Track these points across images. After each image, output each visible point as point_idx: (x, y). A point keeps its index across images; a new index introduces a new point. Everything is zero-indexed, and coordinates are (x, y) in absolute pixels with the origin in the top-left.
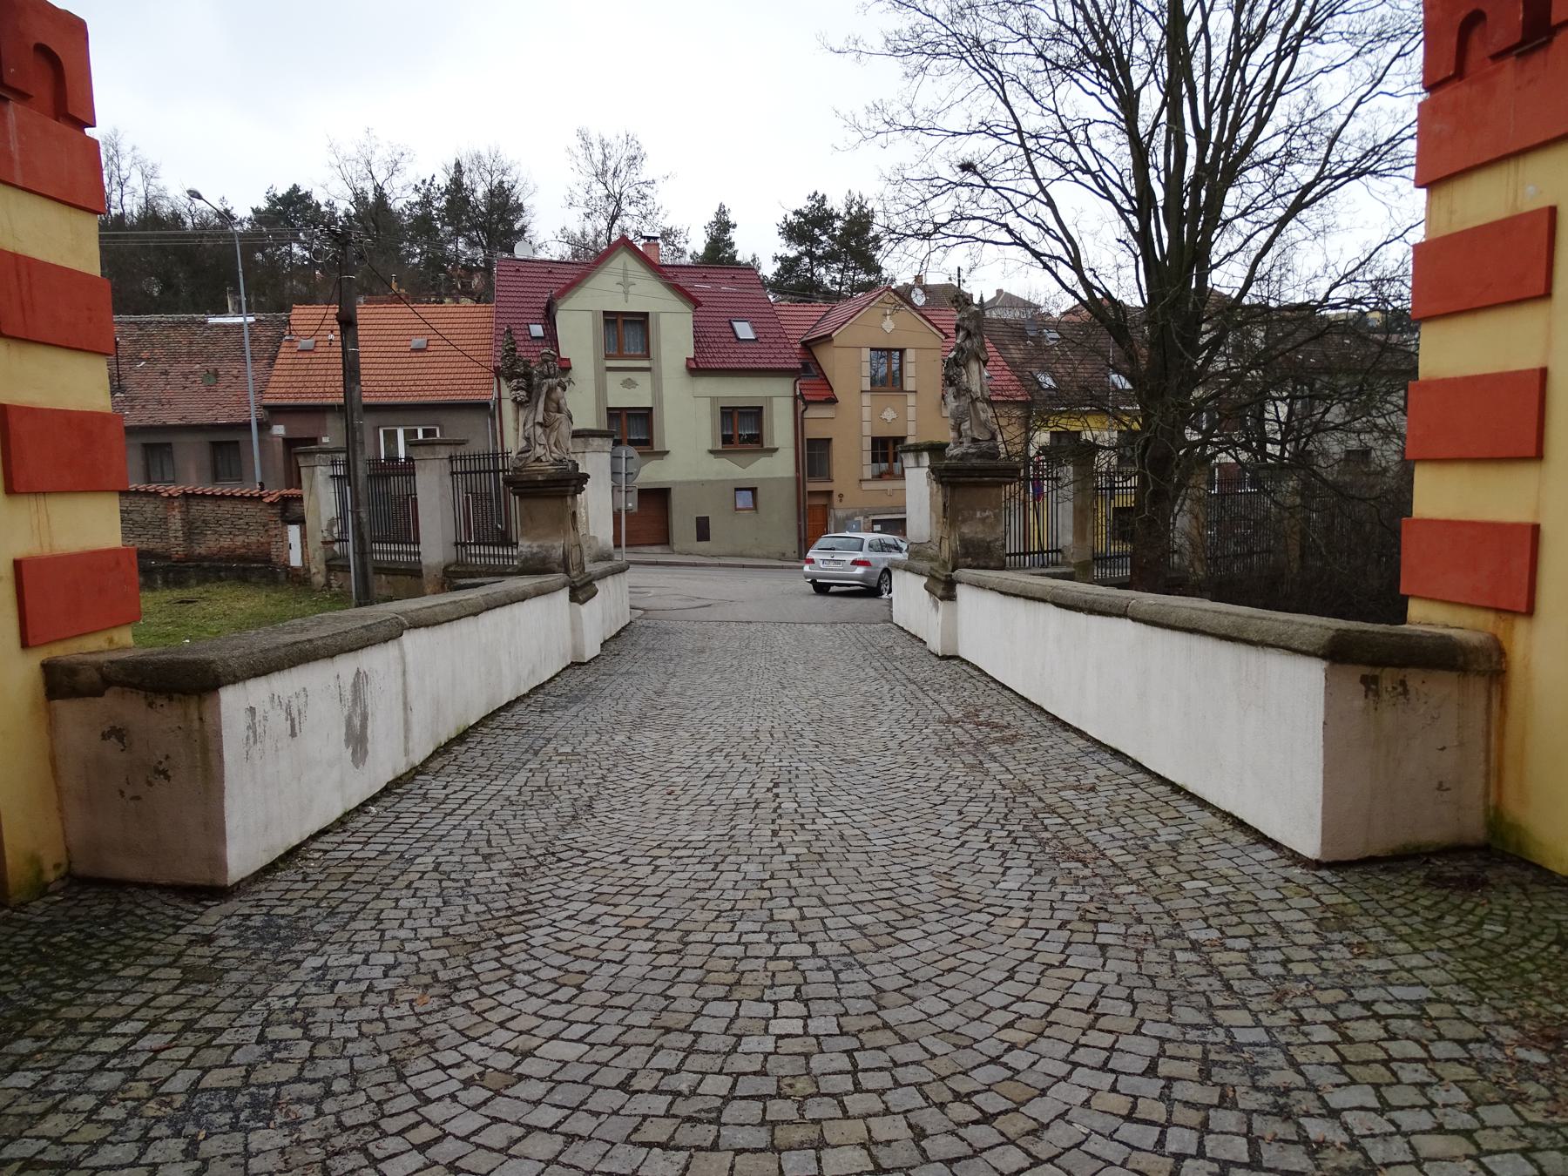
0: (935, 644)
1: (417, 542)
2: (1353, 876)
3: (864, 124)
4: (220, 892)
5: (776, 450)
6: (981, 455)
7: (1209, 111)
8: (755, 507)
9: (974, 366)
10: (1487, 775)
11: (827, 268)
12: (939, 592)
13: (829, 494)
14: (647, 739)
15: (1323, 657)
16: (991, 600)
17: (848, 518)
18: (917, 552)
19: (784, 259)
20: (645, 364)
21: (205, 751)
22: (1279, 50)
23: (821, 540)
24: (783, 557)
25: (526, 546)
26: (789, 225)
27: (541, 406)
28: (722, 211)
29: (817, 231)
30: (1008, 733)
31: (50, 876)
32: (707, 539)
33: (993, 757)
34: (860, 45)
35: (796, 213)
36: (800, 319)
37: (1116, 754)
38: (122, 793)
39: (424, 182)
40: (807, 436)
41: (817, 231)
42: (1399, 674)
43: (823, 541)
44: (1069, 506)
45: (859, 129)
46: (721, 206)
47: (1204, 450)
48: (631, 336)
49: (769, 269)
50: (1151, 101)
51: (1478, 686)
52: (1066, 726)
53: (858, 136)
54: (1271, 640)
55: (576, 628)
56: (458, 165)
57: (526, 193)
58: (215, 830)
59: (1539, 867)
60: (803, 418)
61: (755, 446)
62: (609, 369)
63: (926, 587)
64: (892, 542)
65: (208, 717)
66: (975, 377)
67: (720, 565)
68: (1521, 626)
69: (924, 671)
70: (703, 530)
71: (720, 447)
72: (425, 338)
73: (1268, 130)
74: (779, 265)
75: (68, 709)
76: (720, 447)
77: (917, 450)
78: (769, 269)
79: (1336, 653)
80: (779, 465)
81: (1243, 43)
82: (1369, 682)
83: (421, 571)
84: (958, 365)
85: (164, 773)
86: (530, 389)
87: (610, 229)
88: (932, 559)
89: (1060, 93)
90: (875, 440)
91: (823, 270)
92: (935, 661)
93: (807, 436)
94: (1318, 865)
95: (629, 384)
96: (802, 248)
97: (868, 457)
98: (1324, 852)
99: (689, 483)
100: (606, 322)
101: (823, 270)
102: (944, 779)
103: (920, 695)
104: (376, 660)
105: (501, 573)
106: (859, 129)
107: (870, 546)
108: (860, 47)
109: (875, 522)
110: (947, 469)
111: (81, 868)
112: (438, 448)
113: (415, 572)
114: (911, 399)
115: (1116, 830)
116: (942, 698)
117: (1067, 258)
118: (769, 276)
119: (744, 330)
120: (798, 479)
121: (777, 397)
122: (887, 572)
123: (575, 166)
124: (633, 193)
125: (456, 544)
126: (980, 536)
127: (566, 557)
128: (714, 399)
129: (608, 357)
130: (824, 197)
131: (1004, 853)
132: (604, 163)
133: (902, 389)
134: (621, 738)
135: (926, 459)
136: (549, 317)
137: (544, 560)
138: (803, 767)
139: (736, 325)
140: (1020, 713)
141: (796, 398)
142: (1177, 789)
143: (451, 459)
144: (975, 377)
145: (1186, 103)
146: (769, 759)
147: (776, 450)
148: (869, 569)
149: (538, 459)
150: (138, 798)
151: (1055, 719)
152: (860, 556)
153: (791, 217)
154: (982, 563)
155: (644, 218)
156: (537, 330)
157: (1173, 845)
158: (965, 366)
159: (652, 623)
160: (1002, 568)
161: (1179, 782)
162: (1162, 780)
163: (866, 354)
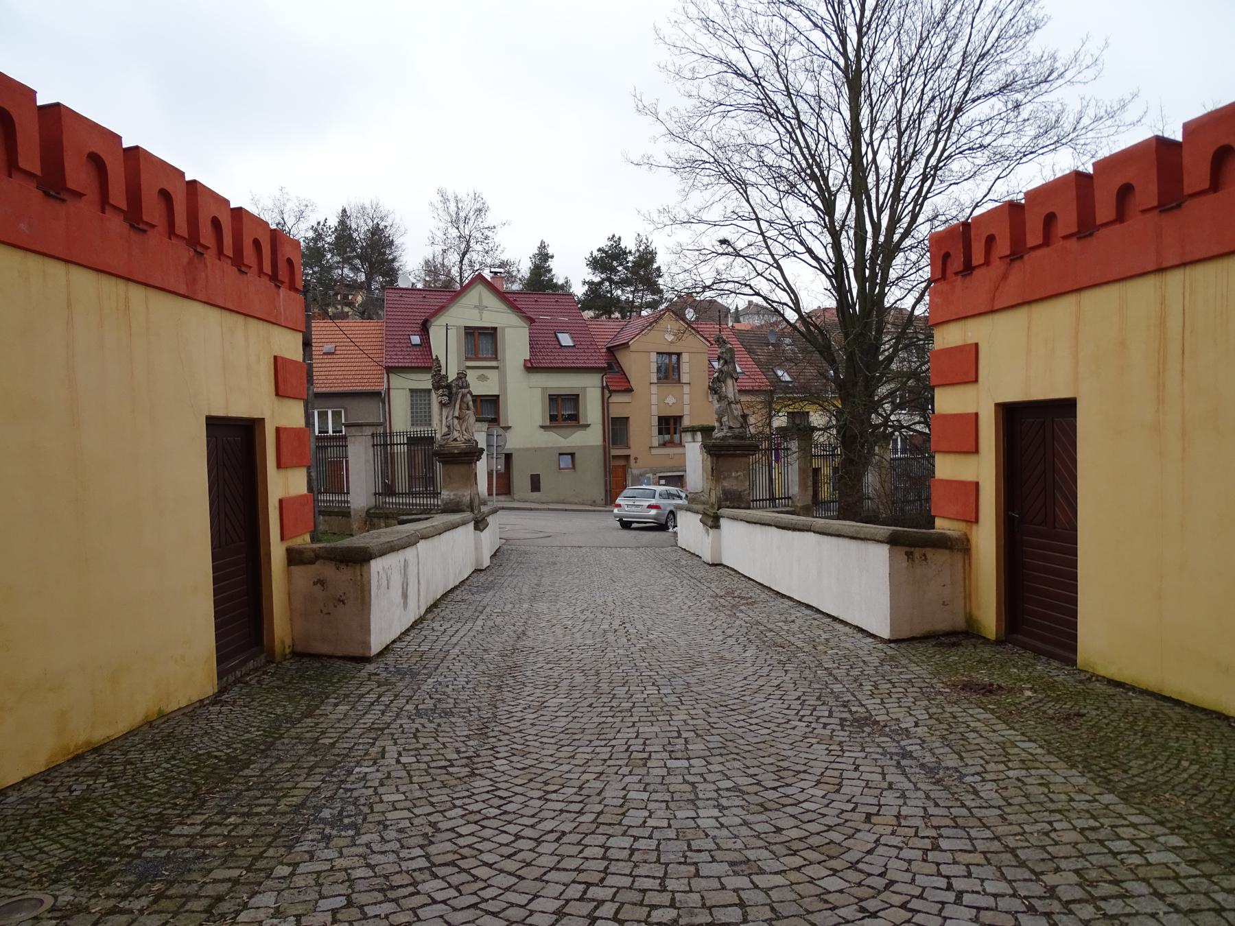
0: (707, 557)
1: (348, 493)
2: (904, 645)
3: (656, 219)
4: (366, 660)
5: (588, 426)
6: (735, 437)
7: (880, 211)
8: (574, 467)
9: (730, 382)
10: (965, 598)
11: (623, 290)
12: (710, 523)
13: (627, 457)
14: (542, 606)
15: (887, 543)
16: (742, 526)
17: (641, 475)
18: (693, 499)
19: (590, 283)
20: (494, 364)
21: (362, 591)
22: (924, 174)
23: (626, 491)
24: (594, 503)
25: (446, 495)
26: (594, 258)
27: (457, 406)
28: (543, 246)
29: (615, 263)
30: (750, 601)
31: (287, 651)
32: (539, 490)
33: (741, 611)
34: (651, 160)
35: (599, 250)
36: (607, 328)
37: (808, 606)
38: (321, 611)
39: (319, 223)
40: (611, 416)
41: (615, 263)
42: (923, 550)
43: (627, 492)
44: (796, 466)
45: (654, 222)
46: (542, 242)
47: (885, 429)
48: (484, 344)
49: (579, 290)
50: (843, 201)
51: (958, 557)
52: (783, 596)
53: (653, 227)
54: (868, 537)
55: (478, 547)
56: (344, 211)
57: (399, 234)
58: (366, 629)
59: (985, 638)
60: (608, 403)
61: (574, 423)
62: (468, 368)
63: (701, 521)
64: (675, 492)
65: (364, 574)
66: (730, 389)
67: (549, 509)
68: (974, 527)
69: (702, 572)
70: (535, 483)
71: (548, 423)
72: (333, 345)
73: (920, 219)
74: (586, 287)
75: (298, 570)
76: (548, 423)
77: (693, 430)
78: (579, 290)
79: (893, 541)
80: (590, 437)
81: (902, 166)
82: (909, 555)
83: (349, 513)
84: (719, 381)
85: (343, 601)
86: (450, 395)
87: (461, 262)
88: (704, 503)
89: (784, 201)
90: (660, 418)
91: (619, 292)
92: (708, 567)
93: (611, 416)
94: (890, 641)
95: (482, 378)
96: (603, 276)
97: (655, 430)
98: (891, 634)
99: (527, 450)
100: (466, 334)
101: (619, 292)
102: (715, 620)
103: (699, 584)
104: (409, 553)
105: (428, 512)
106: (654, 222)
107: (660, 495)
108: (651, 161)
109: (661, 478)
110: (714, 446)
111: (299, 649)
112: (364, 428)
113: (346, 514)
114: (686, 389)
115: (802, 636)
116: (713, 586)
117: (790, 304)
118: (580, 295)
119: (565, 340)
120: (604, 447)
121: (590, 388)
122: (672, 513)
123: (436, 216)
124: (478, 235)
125: (375, 494)
126: (735, 488)
127: (472, 501)
128: (544, 389)
129: (467, 359)
130: (620, 239)
131: (745, 646)
132: (457, 214)
133: (679, 381)
134: (526, 606)
135: (699, 436)
136: (424, 329)
137: (458, 504)
138: (636, 616)
139: (559, 335)
140: (758, 591)
141: (603, 388)
142: (835, 619)
143: (373, 435)
144: (730, 389)
145: (866, 209)
146: (616, 614)
147: (589, 425)
148: (660, 511)
149: (455, 440)
150: (329, 614)
151: (778, 593)
152: (653, 502)
153: (595, 253)
154: (736, 505)
155: (487, 253)
156: (416, 339)
157: (827, 640)
158: (724, 382)
159: (514, 548)
160: (749, 508)
161: (836, 615)
162: (829, 616)
163: (654, 356)
